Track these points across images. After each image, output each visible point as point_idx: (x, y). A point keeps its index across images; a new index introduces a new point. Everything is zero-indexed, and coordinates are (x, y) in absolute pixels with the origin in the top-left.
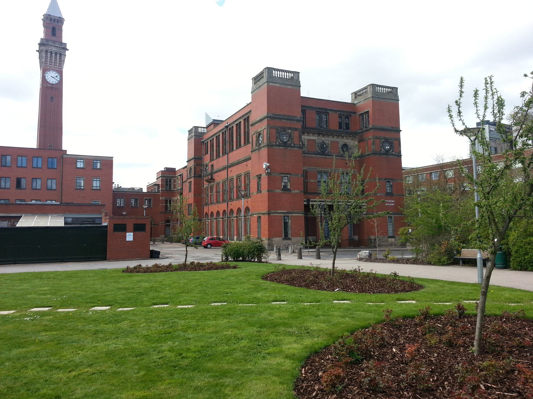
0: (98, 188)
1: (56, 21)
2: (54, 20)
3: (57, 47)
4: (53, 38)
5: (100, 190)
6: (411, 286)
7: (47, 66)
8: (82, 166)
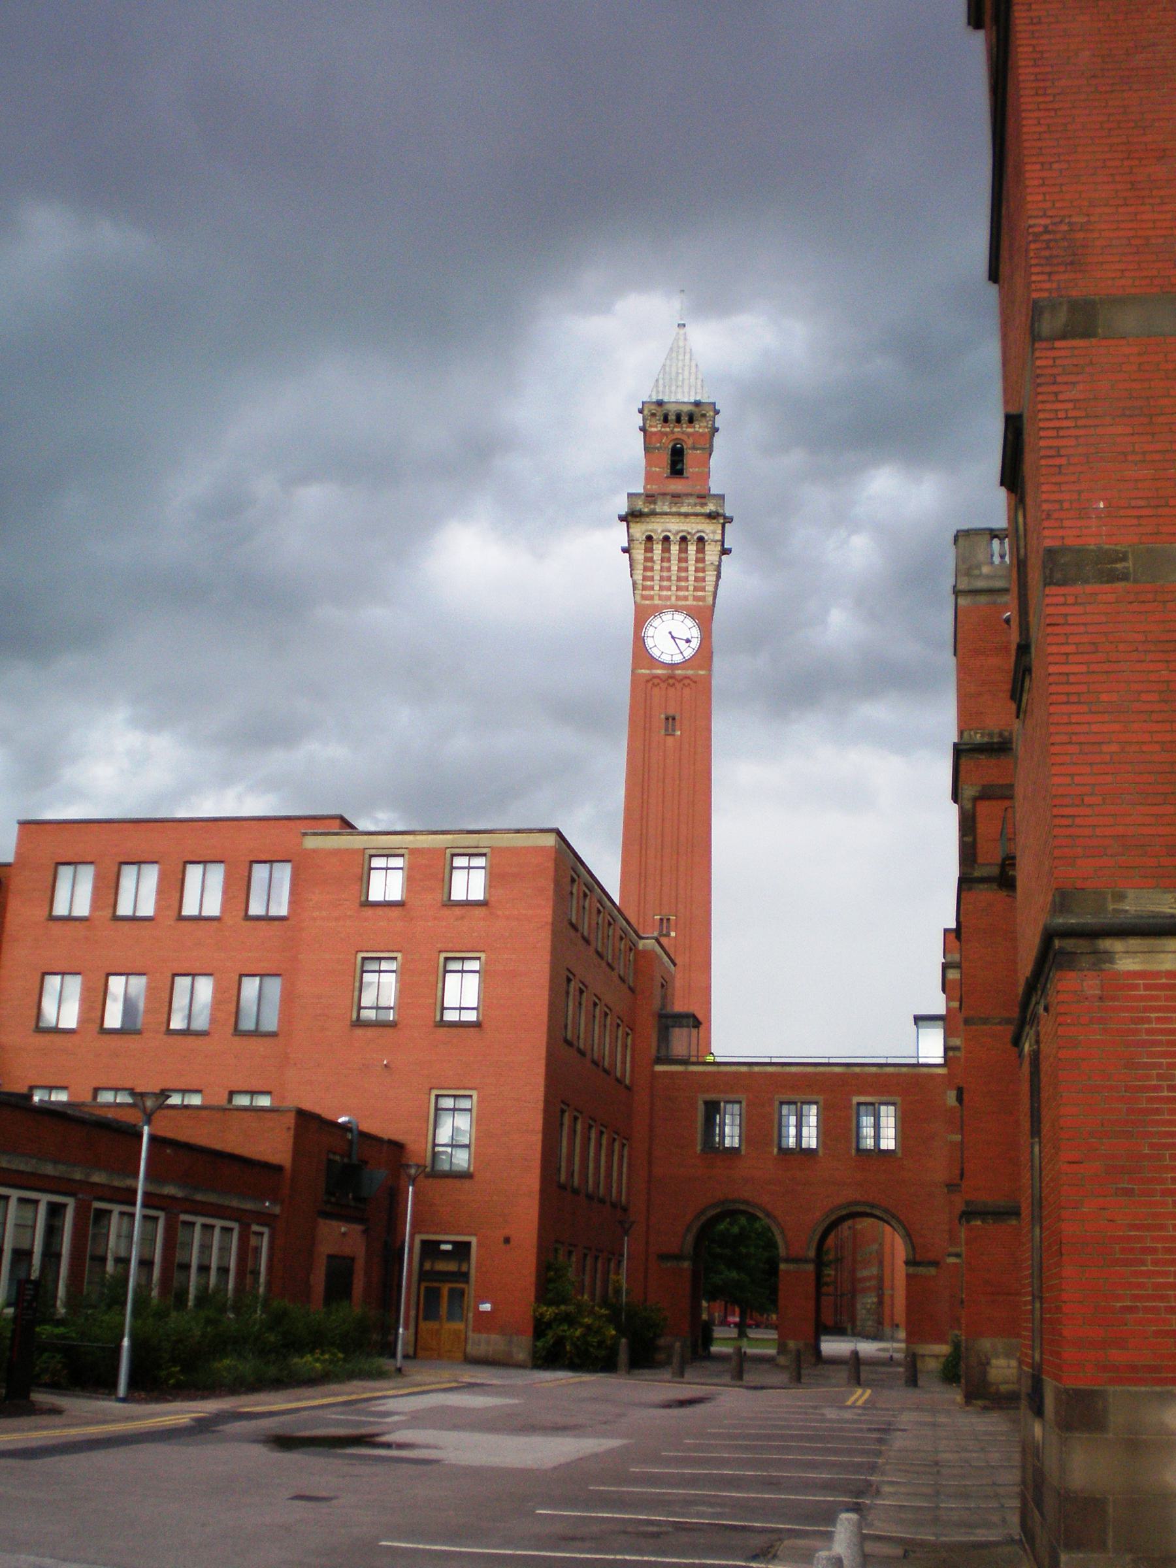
0: (471, 1016)
1: (685, 419)
2: (678, 420)
3: (686, 515)
4: (676, 486)
5: (477, 1025)
6: (379, 1423)
7: (652, 598)
8: (395, 894)
